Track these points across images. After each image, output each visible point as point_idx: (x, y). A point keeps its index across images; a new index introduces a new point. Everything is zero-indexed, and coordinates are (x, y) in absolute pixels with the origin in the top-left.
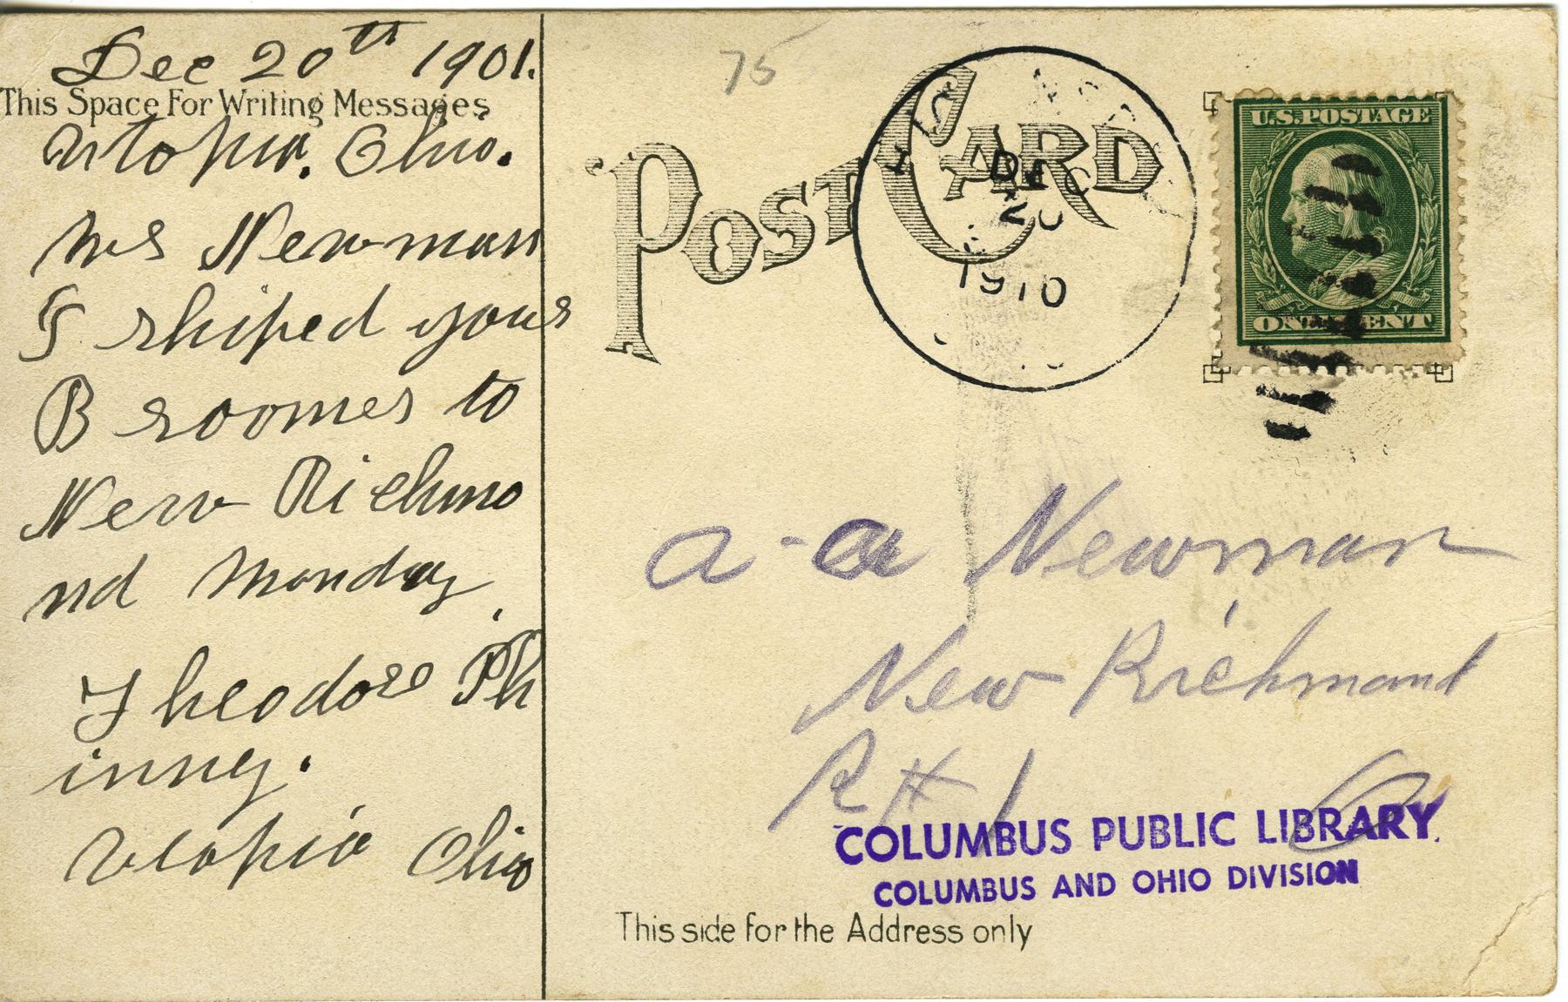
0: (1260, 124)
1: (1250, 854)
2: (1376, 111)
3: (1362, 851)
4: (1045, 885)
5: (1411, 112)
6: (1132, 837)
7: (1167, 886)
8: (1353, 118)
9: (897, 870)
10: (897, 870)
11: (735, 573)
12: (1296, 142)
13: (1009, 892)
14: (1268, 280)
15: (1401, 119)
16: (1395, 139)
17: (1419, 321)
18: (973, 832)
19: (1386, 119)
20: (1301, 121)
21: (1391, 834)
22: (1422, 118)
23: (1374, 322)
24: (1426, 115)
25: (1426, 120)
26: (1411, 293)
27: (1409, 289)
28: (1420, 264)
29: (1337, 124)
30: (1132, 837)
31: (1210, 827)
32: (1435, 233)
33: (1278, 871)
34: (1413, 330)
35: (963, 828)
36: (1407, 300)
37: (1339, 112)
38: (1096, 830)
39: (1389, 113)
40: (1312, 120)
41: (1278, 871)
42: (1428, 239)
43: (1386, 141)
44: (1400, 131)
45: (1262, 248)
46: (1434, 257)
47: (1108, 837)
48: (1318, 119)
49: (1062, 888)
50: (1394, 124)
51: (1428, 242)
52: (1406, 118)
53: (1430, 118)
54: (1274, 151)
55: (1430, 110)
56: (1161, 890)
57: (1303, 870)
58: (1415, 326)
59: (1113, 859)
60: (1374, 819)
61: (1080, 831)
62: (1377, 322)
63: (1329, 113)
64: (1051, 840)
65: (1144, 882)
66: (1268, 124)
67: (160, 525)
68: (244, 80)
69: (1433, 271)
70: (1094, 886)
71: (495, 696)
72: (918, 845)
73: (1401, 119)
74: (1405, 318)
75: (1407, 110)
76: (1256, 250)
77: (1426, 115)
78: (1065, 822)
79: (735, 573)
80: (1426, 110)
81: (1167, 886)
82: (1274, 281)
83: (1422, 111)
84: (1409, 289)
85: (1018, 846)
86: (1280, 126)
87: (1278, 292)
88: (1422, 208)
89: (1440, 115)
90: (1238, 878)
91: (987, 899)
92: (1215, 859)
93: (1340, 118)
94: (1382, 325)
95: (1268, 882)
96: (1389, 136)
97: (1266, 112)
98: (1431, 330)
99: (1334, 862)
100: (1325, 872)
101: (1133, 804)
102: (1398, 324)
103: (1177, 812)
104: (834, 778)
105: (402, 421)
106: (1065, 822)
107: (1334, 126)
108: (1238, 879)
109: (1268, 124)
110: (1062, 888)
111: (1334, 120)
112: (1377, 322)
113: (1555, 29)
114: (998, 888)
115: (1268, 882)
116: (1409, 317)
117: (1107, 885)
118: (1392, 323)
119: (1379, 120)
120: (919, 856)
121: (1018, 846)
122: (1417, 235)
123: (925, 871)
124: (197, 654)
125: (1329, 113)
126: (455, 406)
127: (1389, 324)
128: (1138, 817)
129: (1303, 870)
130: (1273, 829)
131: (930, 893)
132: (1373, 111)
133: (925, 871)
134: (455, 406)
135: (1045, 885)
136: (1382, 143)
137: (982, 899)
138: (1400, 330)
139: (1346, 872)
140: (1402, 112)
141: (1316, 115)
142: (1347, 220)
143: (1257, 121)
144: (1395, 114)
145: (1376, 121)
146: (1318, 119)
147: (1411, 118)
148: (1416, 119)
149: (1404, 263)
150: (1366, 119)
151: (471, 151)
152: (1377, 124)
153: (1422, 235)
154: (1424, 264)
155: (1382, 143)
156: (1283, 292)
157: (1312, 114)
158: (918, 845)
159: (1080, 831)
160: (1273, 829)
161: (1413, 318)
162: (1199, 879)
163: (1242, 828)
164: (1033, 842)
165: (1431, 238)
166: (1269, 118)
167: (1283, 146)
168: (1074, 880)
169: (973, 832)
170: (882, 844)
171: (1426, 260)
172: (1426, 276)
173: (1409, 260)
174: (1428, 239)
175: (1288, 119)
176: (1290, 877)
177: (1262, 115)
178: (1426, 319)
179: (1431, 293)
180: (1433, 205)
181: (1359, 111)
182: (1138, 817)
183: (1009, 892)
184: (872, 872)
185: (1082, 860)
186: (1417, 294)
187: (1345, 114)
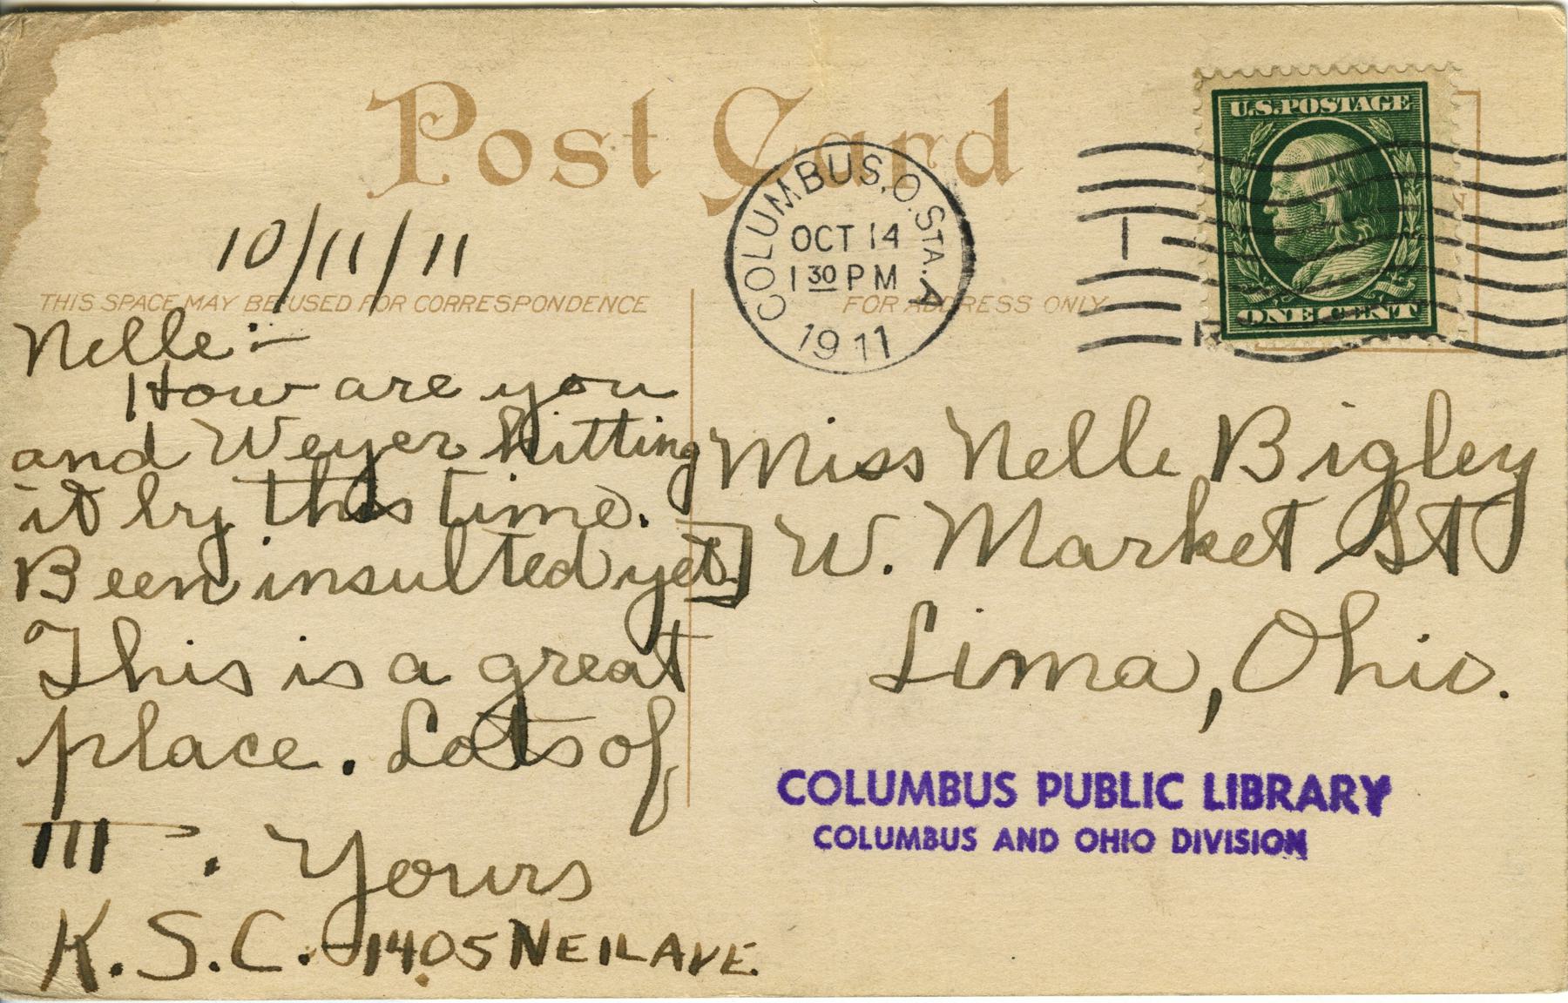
0: (1306, 112)
1: (1195, 817)
2: (1356, 100)
3: (1310, 820)
4: (986, 838)
5: (1391, 100)
6: (1078, 794)
7: (1110, 845)
8: (1333, 107)
9: (840, 814)
10: (840, 814)
12: (1276, 133)
13: (950, 842)
14: (1252, 272)
15: (1381, 107)
16: (1376, 128)
17: (1405, 311)
18: (916, 780)
19: (1366, 108)
20: (1280, 111)
21: (1279, 804)
22: (1403, 106)
23: (1306, 314)
24: (1406, 103)
25: (1407, 108)
26: (1397, 283)
27: (1394, 278)
28: (1404, 253)
29: (1318, 113)
30: (1078, 794)
31: (1158, 790)
33: (1224, 836)
34: (1400, 320)
35: (907, 776)
36: (1394, 290)
37: (1319, 101)
39: (1369, 101)
40: (1292, 110)
41: (1224, 836)
42: (1412, 227)
43: (1367, 130)
44: (1381, 120)
45: (1244, 240)
46: (1417, 246)
47: (1055, 793)
48: (1298, 109)
49: (1003, 841)
50: (1376, 113)
52: (1386, 106)
53: (1411, 106)
54: (1253, 142)
55: (1410, 97)
56: (1104, 850)
57: (1249, 838)
58: (1401, 316)
59: (1060, 817)
60: (1327, 792)
61: (1026, 787)
62: (1310, 314)
63: (1309, 102)
64: (996, 793)
65: (1087, 840)
66: (1248, 115)
67: (1336, 475)
70: (1036, 841)
71: (1356, 672)
72: (860, 790)
73: (1381, 107)
74: (1391, 308)
75: (1387, 97)
76: (1238, 242)
77: (1406, 103)
78: (1011, 776)
80: (1407, 97)
81: (1110, 845)
82: (1257, 273)
83: (1403, 99)
84: (1394, 278)
86: (1260, 117)
87: (1261, 284)
88: (1405, 197)
89: (1220, 124)
90: (1182, 841)
91: (927, 847)
92: (1161, 821)
93: (1320, 105)
94: (1367, 316)
95: (1213, 848)
96: (1370, 125)
97: (1245, 103)
98: (1417, 320)
99: (963, 805)
100: (1272, 841)
101: (1077, 763)
102: (1282, 319)
103: (986, 771)
106: (1011, 776)
107: (1313, 115)
108: (1184, 842)
109: (1248, 115)
110: (1003, 841)
111: (1314, 108)
112: (1310, 314)
114: (938, 837)
115: (1213, 848)
116: (1394, 307)
117: (1049, 840)
118: (1280, 314)
119: (1360, 108)
120: (861, 801)
123: (869, 817)
124: (1310, 625)
125: (1309, 102)
127: (1271, 318)
128: (435, 731)
129: (1249, 838)
130: (1221, 794)
131: (870, 838)
132: (1353, 99)
133: (869, 817)
135: (986, 838)
136: (1363, 131)
137: (922, 846)
138: (1385, 320)
139: (1295, 843)
140: (1383, 100)
141: (1296, 104)
142: (1329, 211)
143: (1235, 111)
144: (1376, 100)
145: (1356, 110)
146: (1298, 109)
147: (1392, 106)
148: (1397, 107)
149: (1388, 253)
150: (1346, 108)
152: (1355, 113)
154: (1408, 254)
155: (1363, 131)
156: (1266, 284)
157: (1291, 104)
158: (860, 790)
159: (1026, 787)
160: (1221, 794)
161: (1398, 308)
162: (1143, 840)
163: (1189, 792)
164: (977, 794)
165: (1415, 227)
166: (1248, 109)
167: (1263, 136)
168: (1017, 833)
169: (916, 780)
170: (825, 788)
171: (1410, 248)
173: (1393, 251)
174: (1412, 227)
175: (1268, 110)
176: (1235, 843)
177: (1241, 106)
178: (1412, 309)
179: (1415, 282)
180: (1416, 192)
181: (1338, 100)
182: (435, 731)
183: (950, 842)
184: (812, 814)
185: (1027, 814)
186: (1402, 284)
187: (1325, 103)
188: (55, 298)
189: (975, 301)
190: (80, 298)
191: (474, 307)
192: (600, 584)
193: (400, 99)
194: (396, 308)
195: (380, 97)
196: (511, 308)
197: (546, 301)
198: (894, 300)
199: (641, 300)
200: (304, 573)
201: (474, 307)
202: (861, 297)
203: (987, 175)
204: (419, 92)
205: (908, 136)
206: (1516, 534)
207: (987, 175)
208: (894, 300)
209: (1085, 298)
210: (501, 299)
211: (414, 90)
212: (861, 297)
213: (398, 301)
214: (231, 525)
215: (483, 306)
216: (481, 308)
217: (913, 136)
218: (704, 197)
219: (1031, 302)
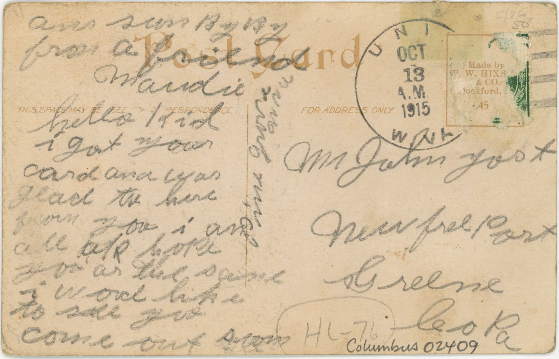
11: (216, 252)
32: (524, 83)
38: (417, 347)
42: (522, 85)
51: (522, 86)
68: (508, 337)
69: (523, 97)
79: (216, 252)
85: (468, 344)
104: (28, 343)
105: (326, 282)
113: (557, 60)
121: (468, 344)
122: (518, 84)
126: (115, 200)
134: (115, 200)
151: (344, 233)
153: (519, 84)
171: (521, 93)
172: (520, 99)
188: (23, 108)
189: (347, 109)
190: (32, 108)
191: (347, 111)
192: (518, 237)
193: (145, 38)
194: (316, 112)
195: (138, 37)
196: (184, 112)
197: (334, 109)
198: (319, 109)
199: (175, 109)
200: (399, 232)
201: (347, 111)
202: (307, 108)
203: (352, 64)
204: (152, 35)
205: (324, 50)
206: (4, 166)
207: (352, 64)
208: (319, 109)
209: (386, 108)
210: (181, 109)
211: (150, 34)
212: (307, 108)
213: (344, 109)
214: (119, 192)
215: (351, 111)
216: (350, 112)
217: (325, 51)
218: (252, 72)
219: (367, 110)
